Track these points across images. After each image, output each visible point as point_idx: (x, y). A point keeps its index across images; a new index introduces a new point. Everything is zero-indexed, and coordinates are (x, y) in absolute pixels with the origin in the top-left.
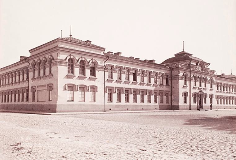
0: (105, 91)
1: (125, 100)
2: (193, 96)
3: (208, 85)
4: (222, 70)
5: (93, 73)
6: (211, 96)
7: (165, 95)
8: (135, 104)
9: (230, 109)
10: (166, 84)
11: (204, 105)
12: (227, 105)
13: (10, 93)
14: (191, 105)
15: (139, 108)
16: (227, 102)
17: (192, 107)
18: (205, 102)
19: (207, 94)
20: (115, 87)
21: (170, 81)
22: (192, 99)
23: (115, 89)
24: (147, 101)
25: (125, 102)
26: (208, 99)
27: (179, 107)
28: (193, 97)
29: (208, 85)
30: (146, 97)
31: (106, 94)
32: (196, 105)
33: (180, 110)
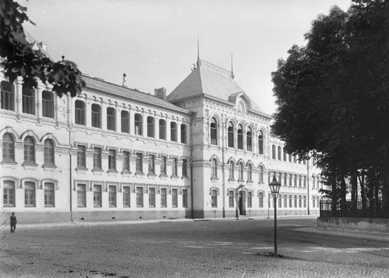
0: (73, 188)
1: (136, 204)
2: (228, 194)
3: (255, 177)
4: (124, 75)
5: (50, 160)
6: (261, 194)
7: (159, 193)
8: (127, 209)
9: (296, 214)
10: (148, 172)
11: (247, 209)
12: (300, 209)
13: (288, 196)
14: (225, 209)
15: (106, 218)
16: (296, 203)
17: (226, 214)
18: (250, 205)
19: (264, 192)
20: (91, 181)
21: (189, 170)
22: (227, 198)
23: (107, 185)
24: (228, 205)
25: (136, 205)
26: (255, 200)
27: (203, 214)
28: (228, 197)
29: (255, 177)
30: (169, 198)
31: (75, 195)
32: (234, 209)
33: (205, 219)
